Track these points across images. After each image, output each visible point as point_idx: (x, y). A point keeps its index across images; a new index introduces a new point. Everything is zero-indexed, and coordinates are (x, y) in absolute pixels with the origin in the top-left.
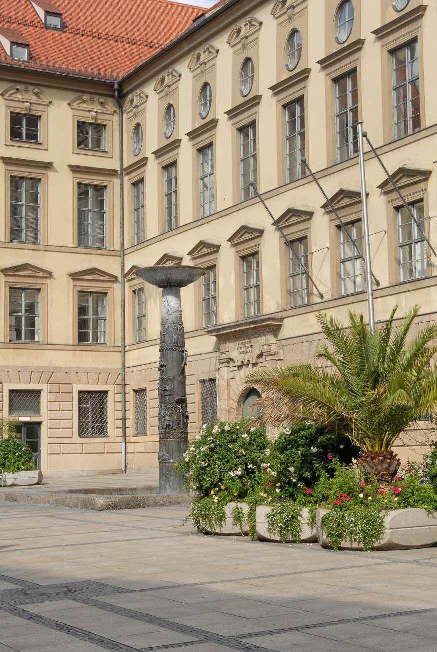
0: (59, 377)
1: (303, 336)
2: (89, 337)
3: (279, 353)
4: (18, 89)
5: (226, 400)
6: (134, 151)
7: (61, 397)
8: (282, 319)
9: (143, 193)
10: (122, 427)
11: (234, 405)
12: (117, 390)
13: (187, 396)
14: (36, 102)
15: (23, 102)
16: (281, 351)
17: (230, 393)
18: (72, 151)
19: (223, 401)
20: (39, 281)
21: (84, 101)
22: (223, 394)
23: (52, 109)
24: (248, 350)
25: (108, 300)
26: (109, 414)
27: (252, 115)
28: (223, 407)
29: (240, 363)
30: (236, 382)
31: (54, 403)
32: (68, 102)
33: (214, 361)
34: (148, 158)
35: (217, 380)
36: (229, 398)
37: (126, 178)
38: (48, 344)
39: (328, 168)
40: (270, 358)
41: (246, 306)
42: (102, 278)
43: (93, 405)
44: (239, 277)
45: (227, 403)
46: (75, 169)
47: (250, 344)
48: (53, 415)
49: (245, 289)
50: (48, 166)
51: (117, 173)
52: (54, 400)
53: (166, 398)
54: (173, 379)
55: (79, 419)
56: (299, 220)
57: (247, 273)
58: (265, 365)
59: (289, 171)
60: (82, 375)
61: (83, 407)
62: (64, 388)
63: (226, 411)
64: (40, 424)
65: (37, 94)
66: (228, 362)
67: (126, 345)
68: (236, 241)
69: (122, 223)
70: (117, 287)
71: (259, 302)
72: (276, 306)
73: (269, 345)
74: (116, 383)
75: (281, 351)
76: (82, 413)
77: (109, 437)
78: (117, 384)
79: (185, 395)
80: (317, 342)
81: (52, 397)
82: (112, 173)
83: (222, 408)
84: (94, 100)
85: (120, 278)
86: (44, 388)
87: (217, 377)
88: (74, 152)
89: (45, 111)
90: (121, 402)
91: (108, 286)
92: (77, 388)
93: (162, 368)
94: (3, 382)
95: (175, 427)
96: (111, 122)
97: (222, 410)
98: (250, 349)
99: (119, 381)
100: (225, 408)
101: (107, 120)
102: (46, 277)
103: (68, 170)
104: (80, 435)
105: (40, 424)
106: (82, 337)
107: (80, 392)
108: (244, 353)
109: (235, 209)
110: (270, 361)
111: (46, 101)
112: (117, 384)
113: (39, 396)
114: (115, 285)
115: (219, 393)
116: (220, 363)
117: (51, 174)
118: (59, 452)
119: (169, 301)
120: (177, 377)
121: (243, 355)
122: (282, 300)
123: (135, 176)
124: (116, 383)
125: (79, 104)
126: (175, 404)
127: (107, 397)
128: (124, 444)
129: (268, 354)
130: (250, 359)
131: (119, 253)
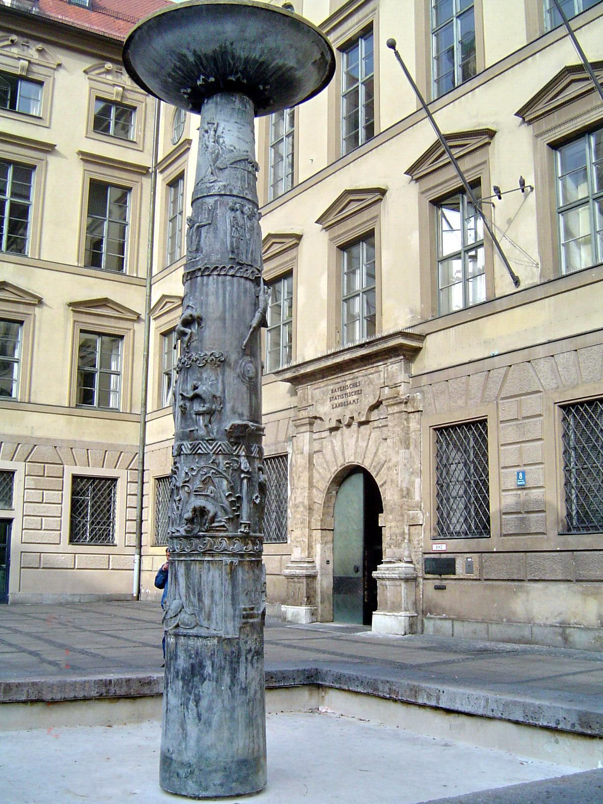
0: (45, 453)
1: (470, 362)
2: (92, 397)
3: (414, 399)
4: (12, 41)
5: (304, 488)
6: (172, 140)
7: (45, 482)
8: (421, 337)
9: (182, 195)
10: (135, 531)
11: (319, 498)
12: (131, 477)
13: (264, 420)
14: (37, 62)
15: (19, 59)
16: (419, 396)
17: (312, 476)
18: (84, 135)
19: (299, 491)
20: (22, 309)
21: (108, 72)
22: (299, 477)
23: (60, 75)
24: (350, 399)
25: (123, 346)
26: (118, 512)
27: (367, 15)
28: (299, 500)
29: (334, 424)
30: (324, 458)
31: (33, 491)
32: (85, 68)
33: (283, 425)
34: (192, 140)
35: (289, 457)
36: (311, 485)
37: (160, 177)
38: (29, 403)
39: (527, 45)
40: (396, 409)
41: (345, 327)
42: (116, 314)
43: (93, 498)
44: (336, 280)
45: (307, 495)
46: (88, 158)
47: (356, 389)
48: (30, 509)
49: (345, 301)
50: (48, 149)
51: (148, 171)
52: (34, 487)
53: (196, 423)
54: (221, 363)
55: (71, 516)
56: (462, 153)
57: (348, 274)
58: (385, 423)
59: (436, 85)
60: (79, 453)
61: (78, 501)
63: (304, 507)
64: (10, 521)
65: (40, 51)
66: (311, 424)
67: (148, 412)
68: (332, 220)
69: (150, 239)
70: (140, 328)
71: (371, 320)
72: (410, 316)
73: (396, 386)
74: (130, 468)
75: (419, 396)
76: (76, 507)
77: (116, 546)
78: (131, 469)
79: (255, 414)
80: (503, 371)
81: (31, 482)
82: (143, 171)
83: (297, 502)
84: (121, 73)
85: (143, 317)
86: (19, 468)
87: (290, 450)
88: (88, 136)
89: (50, 77)
90: (136, 495)
91: (126, 327)
92: (70, 470)
93: (188, 330)
95: (222, 519)
96: (144, 104)
97: (296, 506)
98: (355, 397)
99: (135, 464)
100: (303, 503)
101: (139, 101)
102: (34, 305)
103: (77, 158)
104: (71, 541)
105: (10, 521)
106: (85, 397)
107: (75, 478)
108: (341, 405)
109: (331, 170)
110: (396, 415)
112: (131, 469)
113: (12, 480)
114: (136, 325)
115: (292, 477)
116: (297, 426)
117: (51, 159)
118: (37, 566)
119: (220, 130)
120: (233, 357)
121: (339, 409)
122: (422, 303)
123: (172, 172)
124: (130, 468)
125: (100, 74)
126: (223, 444)
127: (115, 486)
128: (137, 557)
129: (391, 402)
130: (355, 415)
131: (143, 282)
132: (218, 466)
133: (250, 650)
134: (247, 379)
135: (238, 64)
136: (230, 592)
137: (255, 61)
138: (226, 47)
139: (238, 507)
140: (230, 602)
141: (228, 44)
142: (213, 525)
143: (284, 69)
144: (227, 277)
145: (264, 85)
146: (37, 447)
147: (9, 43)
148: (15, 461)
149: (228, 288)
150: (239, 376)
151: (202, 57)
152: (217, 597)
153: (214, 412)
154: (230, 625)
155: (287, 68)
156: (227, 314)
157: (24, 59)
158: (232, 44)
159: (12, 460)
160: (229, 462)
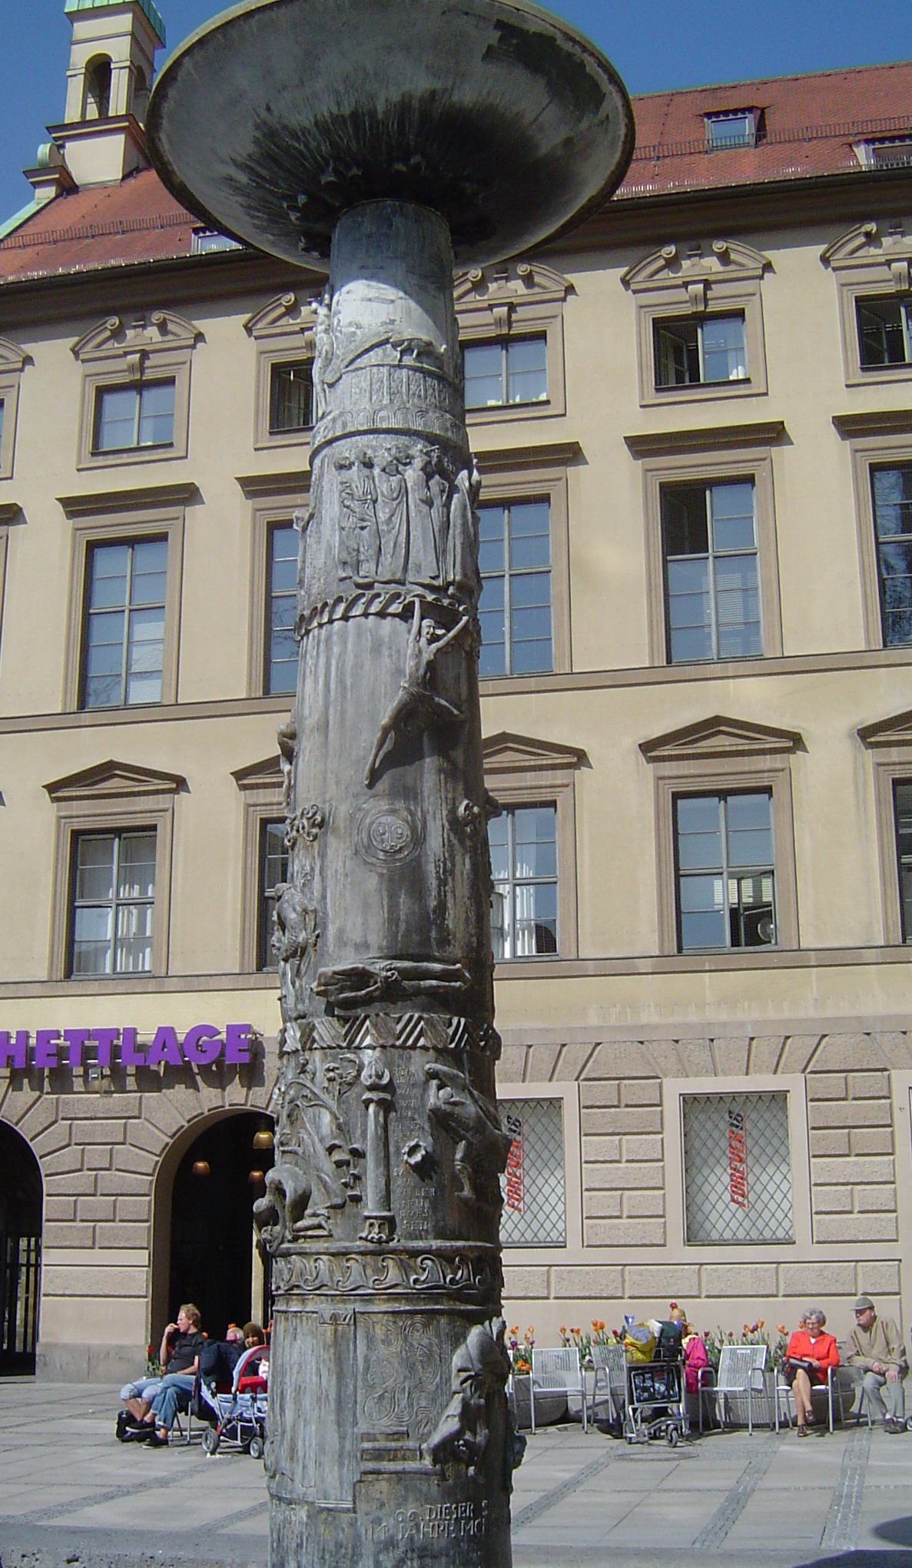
4: (868, 235)
14: (720, 277)
46: (850, 426)
62: (635, 1091)
78: (812, 1072)
92: (674, 1088)
94: (889, 1067)
111: (556, 290)
112: (812, 1072)
117: (193, 512)
132: (312, 1080)
133: (390, 1544)
134: (381, 855)
135: (313, 144)
136: (333, 1396)
137: (338, 120)
138: (265, 123)
139: (357, 1178)
140: (333, 1417)
141: (264, 114)
142: (300, 1224)
143: (415, 104)
144: (336, 623)
145: (405, 159)
146: (791, 1039)
147: (862, 239)
148: (557, 1081)
149: (336, 650)
150: (356, 853)
151: (248, 162)
152: (307, 1402)
153: (304, 950)
154: (331, 1475)
155: (422, 99)
156: (331, 711)
157: (899, 260)
158: (268, 109)
159: (747, 1074)
160: (332, 1065)
